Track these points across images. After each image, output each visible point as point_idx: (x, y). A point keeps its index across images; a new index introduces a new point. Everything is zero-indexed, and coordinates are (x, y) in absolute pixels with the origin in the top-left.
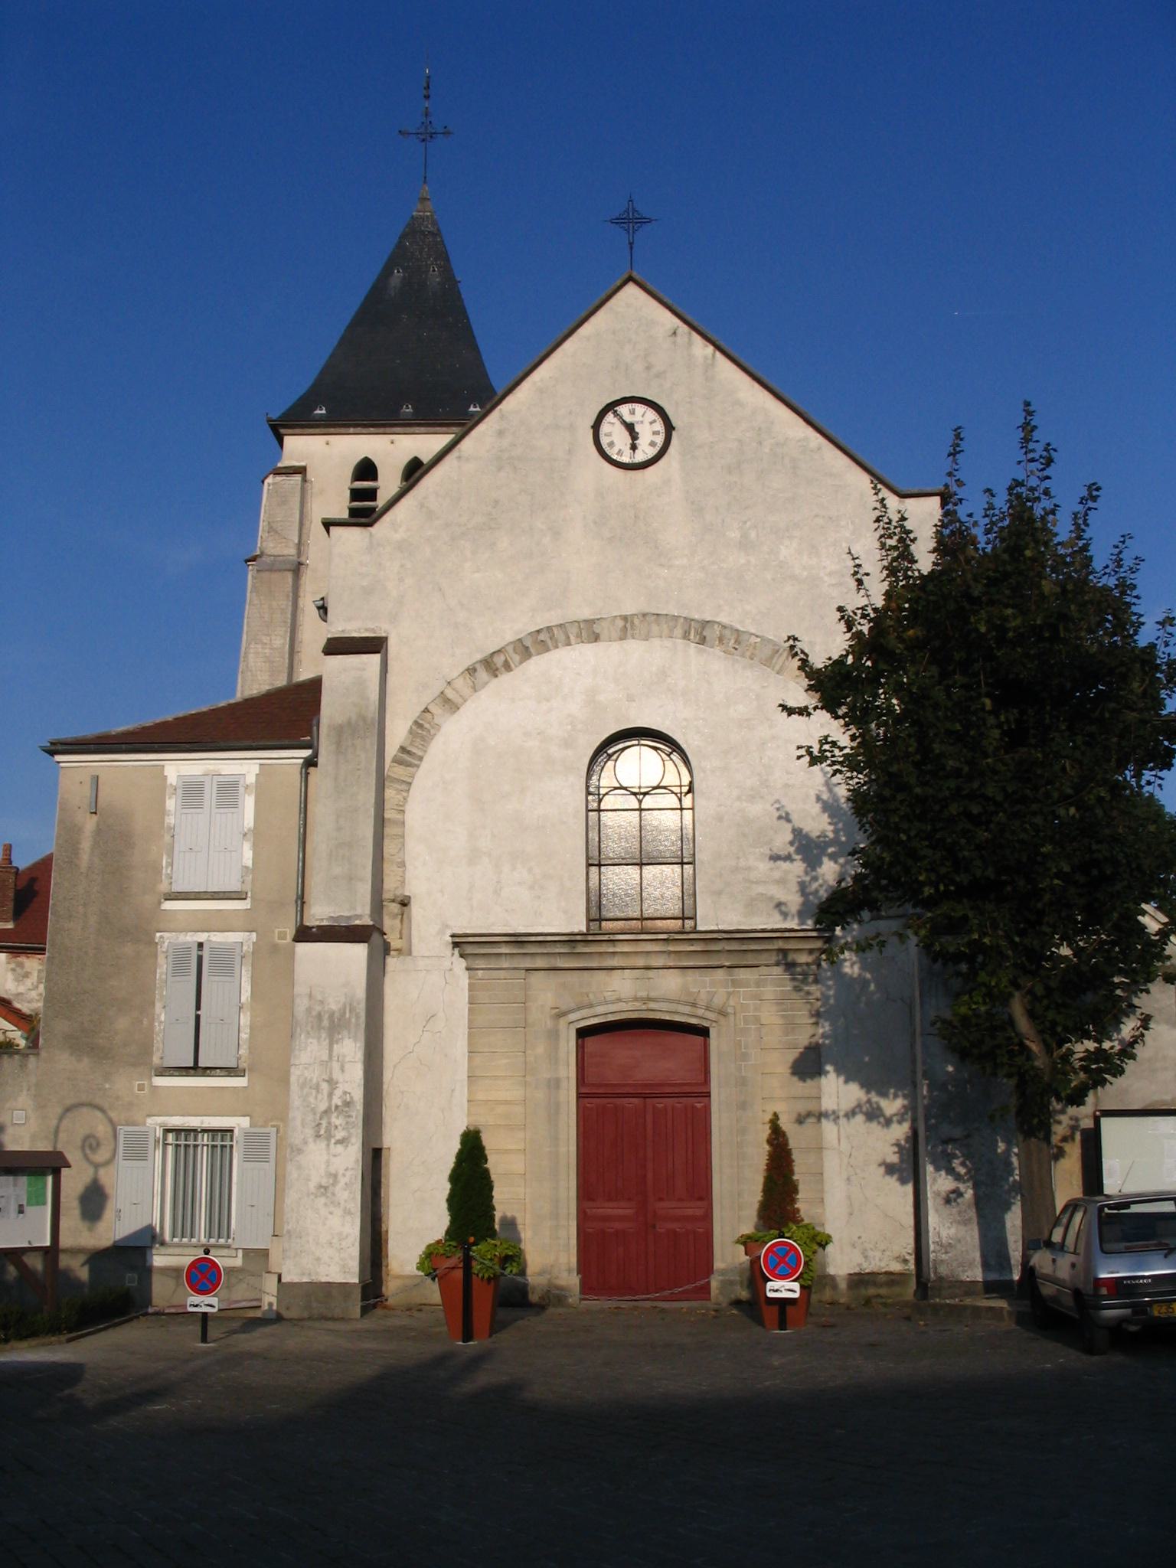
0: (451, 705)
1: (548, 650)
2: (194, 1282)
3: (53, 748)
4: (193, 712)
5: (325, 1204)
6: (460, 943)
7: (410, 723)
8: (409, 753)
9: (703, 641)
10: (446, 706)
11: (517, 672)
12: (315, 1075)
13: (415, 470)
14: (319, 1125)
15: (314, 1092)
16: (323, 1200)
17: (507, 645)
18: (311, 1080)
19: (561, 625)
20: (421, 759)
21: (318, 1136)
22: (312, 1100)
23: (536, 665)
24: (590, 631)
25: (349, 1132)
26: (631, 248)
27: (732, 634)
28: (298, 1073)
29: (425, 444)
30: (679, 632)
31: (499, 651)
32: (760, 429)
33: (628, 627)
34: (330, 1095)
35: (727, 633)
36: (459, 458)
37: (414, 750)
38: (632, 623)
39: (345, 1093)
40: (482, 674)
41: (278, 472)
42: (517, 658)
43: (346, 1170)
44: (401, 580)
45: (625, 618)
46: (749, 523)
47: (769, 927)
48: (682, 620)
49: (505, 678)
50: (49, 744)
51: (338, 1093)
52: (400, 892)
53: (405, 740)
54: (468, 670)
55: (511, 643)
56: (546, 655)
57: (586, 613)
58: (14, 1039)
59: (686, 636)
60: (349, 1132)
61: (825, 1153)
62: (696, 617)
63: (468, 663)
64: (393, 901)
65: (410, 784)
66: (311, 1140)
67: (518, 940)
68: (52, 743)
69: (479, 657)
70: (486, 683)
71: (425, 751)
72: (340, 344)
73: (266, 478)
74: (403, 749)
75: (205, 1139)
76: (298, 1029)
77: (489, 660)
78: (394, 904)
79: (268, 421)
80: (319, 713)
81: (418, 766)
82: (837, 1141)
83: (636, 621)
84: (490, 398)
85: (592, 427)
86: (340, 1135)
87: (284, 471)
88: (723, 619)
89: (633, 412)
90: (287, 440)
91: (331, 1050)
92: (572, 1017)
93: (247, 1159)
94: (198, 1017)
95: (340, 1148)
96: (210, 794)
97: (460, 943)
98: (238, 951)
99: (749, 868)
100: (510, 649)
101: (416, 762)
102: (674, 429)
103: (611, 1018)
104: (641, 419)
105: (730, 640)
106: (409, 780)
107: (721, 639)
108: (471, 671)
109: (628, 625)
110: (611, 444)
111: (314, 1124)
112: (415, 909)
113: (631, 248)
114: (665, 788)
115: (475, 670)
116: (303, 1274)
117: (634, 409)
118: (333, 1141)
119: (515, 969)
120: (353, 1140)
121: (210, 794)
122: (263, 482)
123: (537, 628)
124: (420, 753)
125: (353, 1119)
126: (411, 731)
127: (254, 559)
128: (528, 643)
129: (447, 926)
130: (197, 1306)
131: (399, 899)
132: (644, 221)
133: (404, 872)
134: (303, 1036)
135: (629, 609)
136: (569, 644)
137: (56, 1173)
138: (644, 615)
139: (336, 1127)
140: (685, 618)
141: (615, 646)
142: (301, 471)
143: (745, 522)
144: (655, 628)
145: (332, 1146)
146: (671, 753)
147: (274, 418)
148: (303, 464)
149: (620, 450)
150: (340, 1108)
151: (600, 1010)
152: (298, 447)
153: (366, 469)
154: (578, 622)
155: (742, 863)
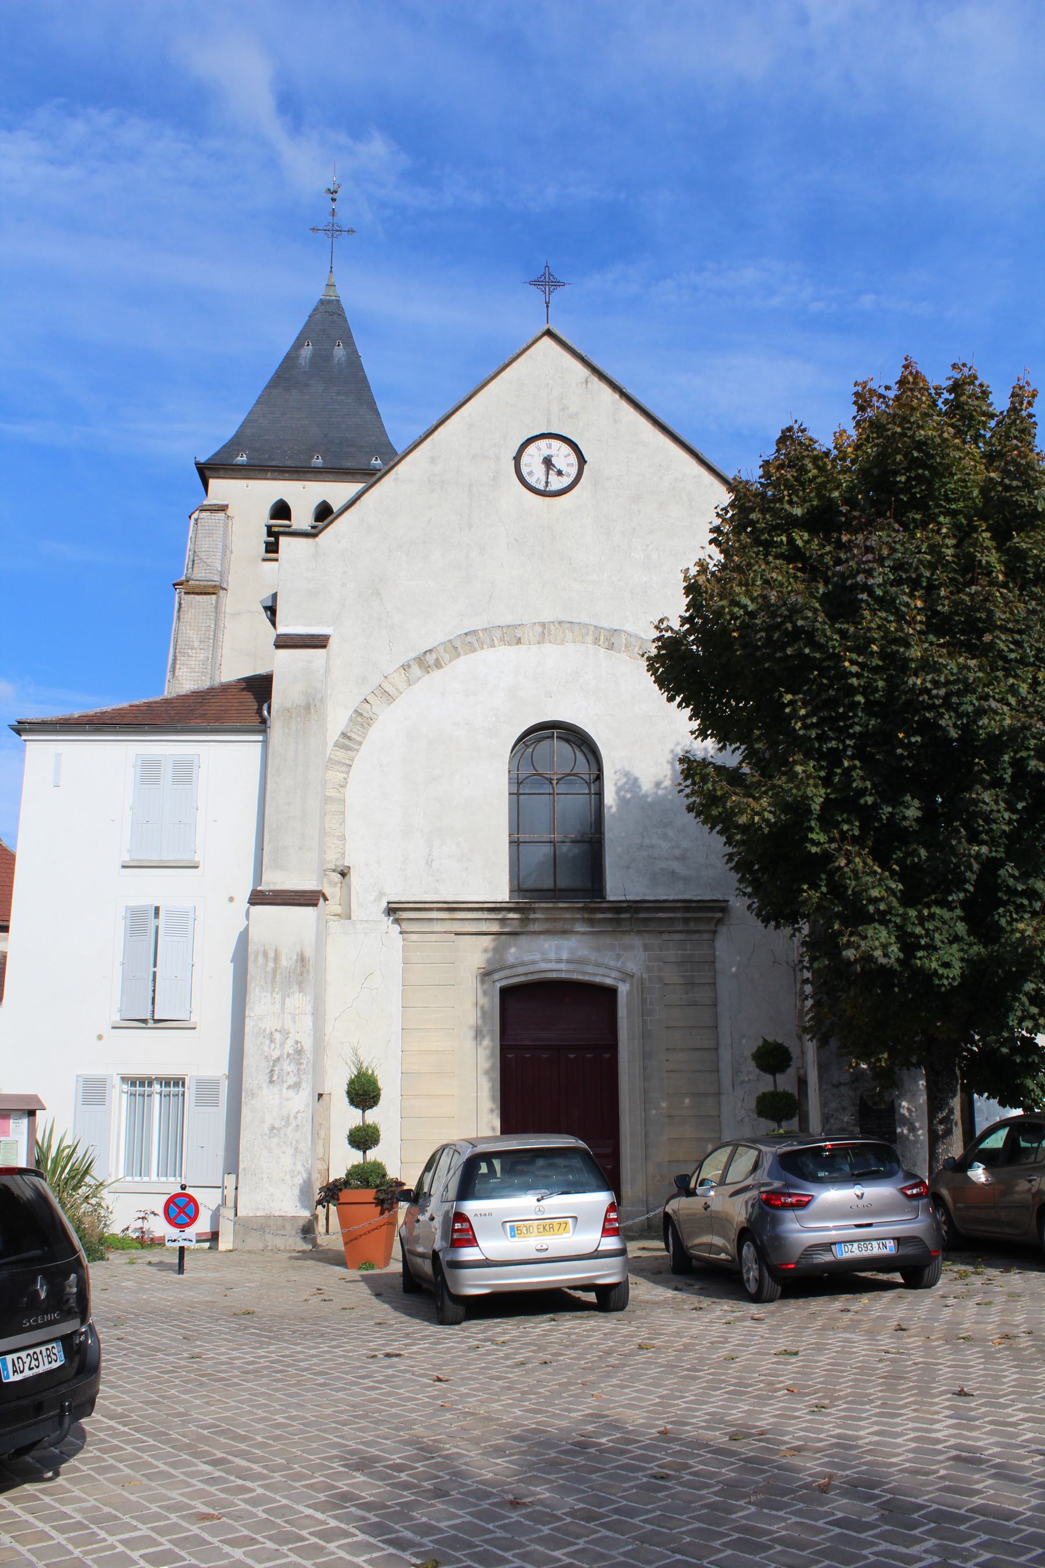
0: (389, 698)
1: (475, 650)
2: (172, 1215)
3: (21, 726)
4: (137, 703)
5: (278, 1144)
6: (392, 910)
7: (351, 712)
8: (349, 738)
9: (611, 647)
10: (384, 697)
11: (447, 669)
12: (270, 1025)
13: (324, 513)
14: (272, 1071)
15: (267, 1042)
16: (275, 1140)
17: (439, 645)
18: (265, 1030)
19: (485, 630)
20: (360, 744)
21: (271, 1082)
22: (266, 1048)
23: (464, 663)
24: (512, 636)
25: (299, 1077)
26: (547, 306)
27: (637, 642)
28: (252, 1023)
29: (337, 492)
30: (590, 639)
31: (431, 651)
32: (660, 465)
33: (545, 631)
34: (282, 1044)
35: (633, 640)
36: (396, 479)
37: (353, 736)
38: (549, 629)
39: (297, 1042)
40: (416, 670)
41: (203, 509)
42: (447, 657)
43: (298, 1112)
44: (344, 585)
45: (543, 625)
46: (651, 546)
47: (671, 898)
48: (592, 628)
49: (436, 674)
50: (16, 724)
51: (290, 1042)
52: (342, 862)
53: (346, 727)
54: (403, 666)
55: (441, 643)
56: (472, 655)
57: (508, 619)
58: (916, 363)
59: (596, 641)
60: (299, 1077)
61: (723, 1097)
62: (606, 625)
63: (403, 660)
64: (334, 871)
65: (350, 766)
66: (265, 1085)
67: (451, 907)
68: (19, 723)
69: (413, 655)
70: (419, 679)
71: (364, 738)
72: (258, 402)
73: (192, 514)
74: (344, 735)
75: (157, 1087)
76: (253, 984)
77: (422, 658)
78: (335, 874)
79: (196, 464)
80: (270, 698)
81: (358, 751)
82: (731, 1087)
83: (552, 628)
84: (392, 458)
85: (514, 458)
86: (291, 1080)
87: (209, 508)
88: (629, 628)
89: (550, 447)
90: (212, 482)
91: (283, 1004)
92: (496, 976)
93: (199, 1103)
94: (155, 973)
95: (291, 1093)
96: (167, 773)
97: (392, 910)
98: (192, 914)
99: (652, 847)
100: (441, 649)
101: (356, 747)
102: (585, 462)
103: (530, 977)
104: (557, 453)
105: (635, 646)
106: (350, 763)
107: (627, 646)
108: (406, 667)
109: (546, 632)
110: (531, 473)
111: (268, 1071)
112: (353, 876)
113: (547, 306)
114: (575, 775)
115: (409, 666)
116: (257, 1209)
117: (551, 444)
118: (285, 1086)
119: (446, 932)
120: (304, 1085)
121: (167, 773)
122: (190, 517)
123: (466, 631)
124: (359, 739)
125: (304, 1066)
126: (351, 720)
127: (181, 584)
128: (457, 644)
129: (382, 894)
130: (175, 1241)
131: (339, 869)
132: (558, 284)
133: (344, 845)
134: (257, 990)
135: (547, 617)
136: (493, 646)
137: (32, 1113)
138: (560, 623)
139: (289, 1073)
140: (595, 626)
141: (534, 648)
142: (223, 508)
143: (648, 546)
144: (569, 635)
145: (284, 1090)
146: (581, 745)
147: (202, 462)
148: (226, 503)
149: (538, 479)
150: (292, 1057)
151: (521, 970)
152: (221, 489)
153: (281, 510)
154: (502, 627)
155: (647, 841)
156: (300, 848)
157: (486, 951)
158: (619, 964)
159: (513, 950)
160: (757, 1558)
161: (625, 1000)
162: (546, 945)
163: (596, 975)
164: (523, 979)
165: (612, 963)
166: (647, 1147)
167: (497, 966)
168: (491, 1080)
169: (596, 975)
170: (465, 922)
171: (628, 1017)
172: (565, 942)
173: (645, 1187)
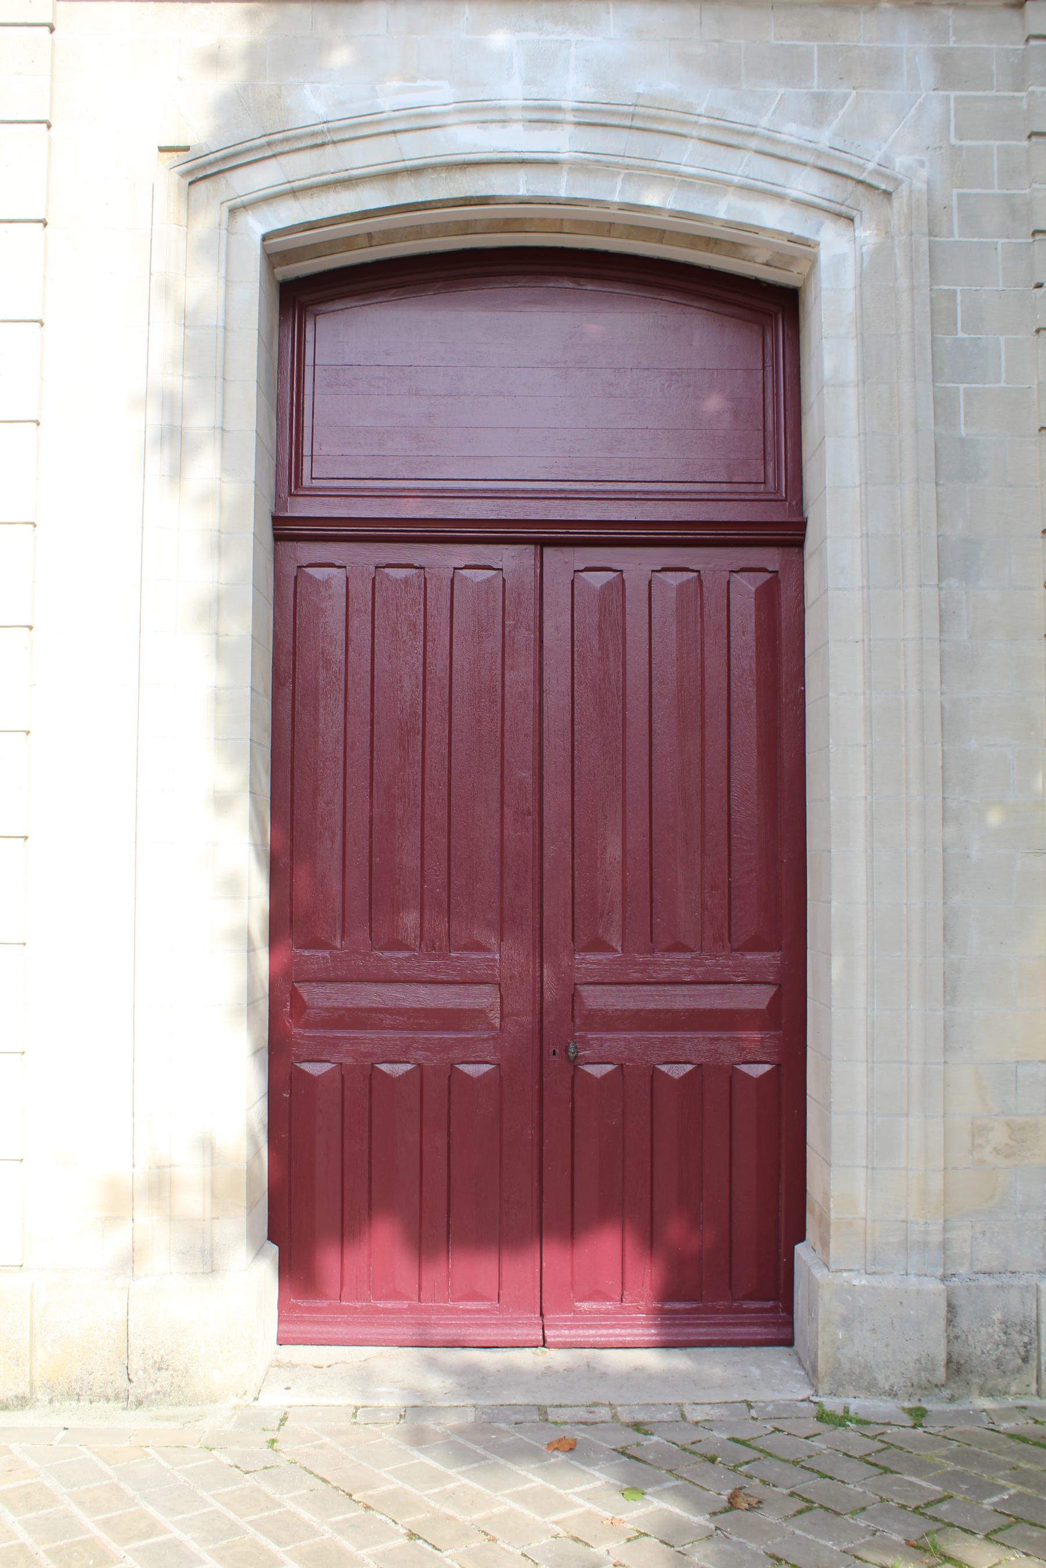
103: (407, 192)
156: (966, 769)
157: (215, 60)
158: (825, 138)
159: (341, 57)
160: (400, 1484)
161: (849, 303)
162: (500, 39)
163: (717, 185)
164: (371, 198)
165: (792, 131)
166: (951, 992)
167: (248, 130)
168: (221, 652)
169: (717, 185)
170: (608, 129)
171: (865, 377)
172: (573, 36)
173: (937, 1183)
